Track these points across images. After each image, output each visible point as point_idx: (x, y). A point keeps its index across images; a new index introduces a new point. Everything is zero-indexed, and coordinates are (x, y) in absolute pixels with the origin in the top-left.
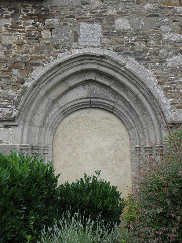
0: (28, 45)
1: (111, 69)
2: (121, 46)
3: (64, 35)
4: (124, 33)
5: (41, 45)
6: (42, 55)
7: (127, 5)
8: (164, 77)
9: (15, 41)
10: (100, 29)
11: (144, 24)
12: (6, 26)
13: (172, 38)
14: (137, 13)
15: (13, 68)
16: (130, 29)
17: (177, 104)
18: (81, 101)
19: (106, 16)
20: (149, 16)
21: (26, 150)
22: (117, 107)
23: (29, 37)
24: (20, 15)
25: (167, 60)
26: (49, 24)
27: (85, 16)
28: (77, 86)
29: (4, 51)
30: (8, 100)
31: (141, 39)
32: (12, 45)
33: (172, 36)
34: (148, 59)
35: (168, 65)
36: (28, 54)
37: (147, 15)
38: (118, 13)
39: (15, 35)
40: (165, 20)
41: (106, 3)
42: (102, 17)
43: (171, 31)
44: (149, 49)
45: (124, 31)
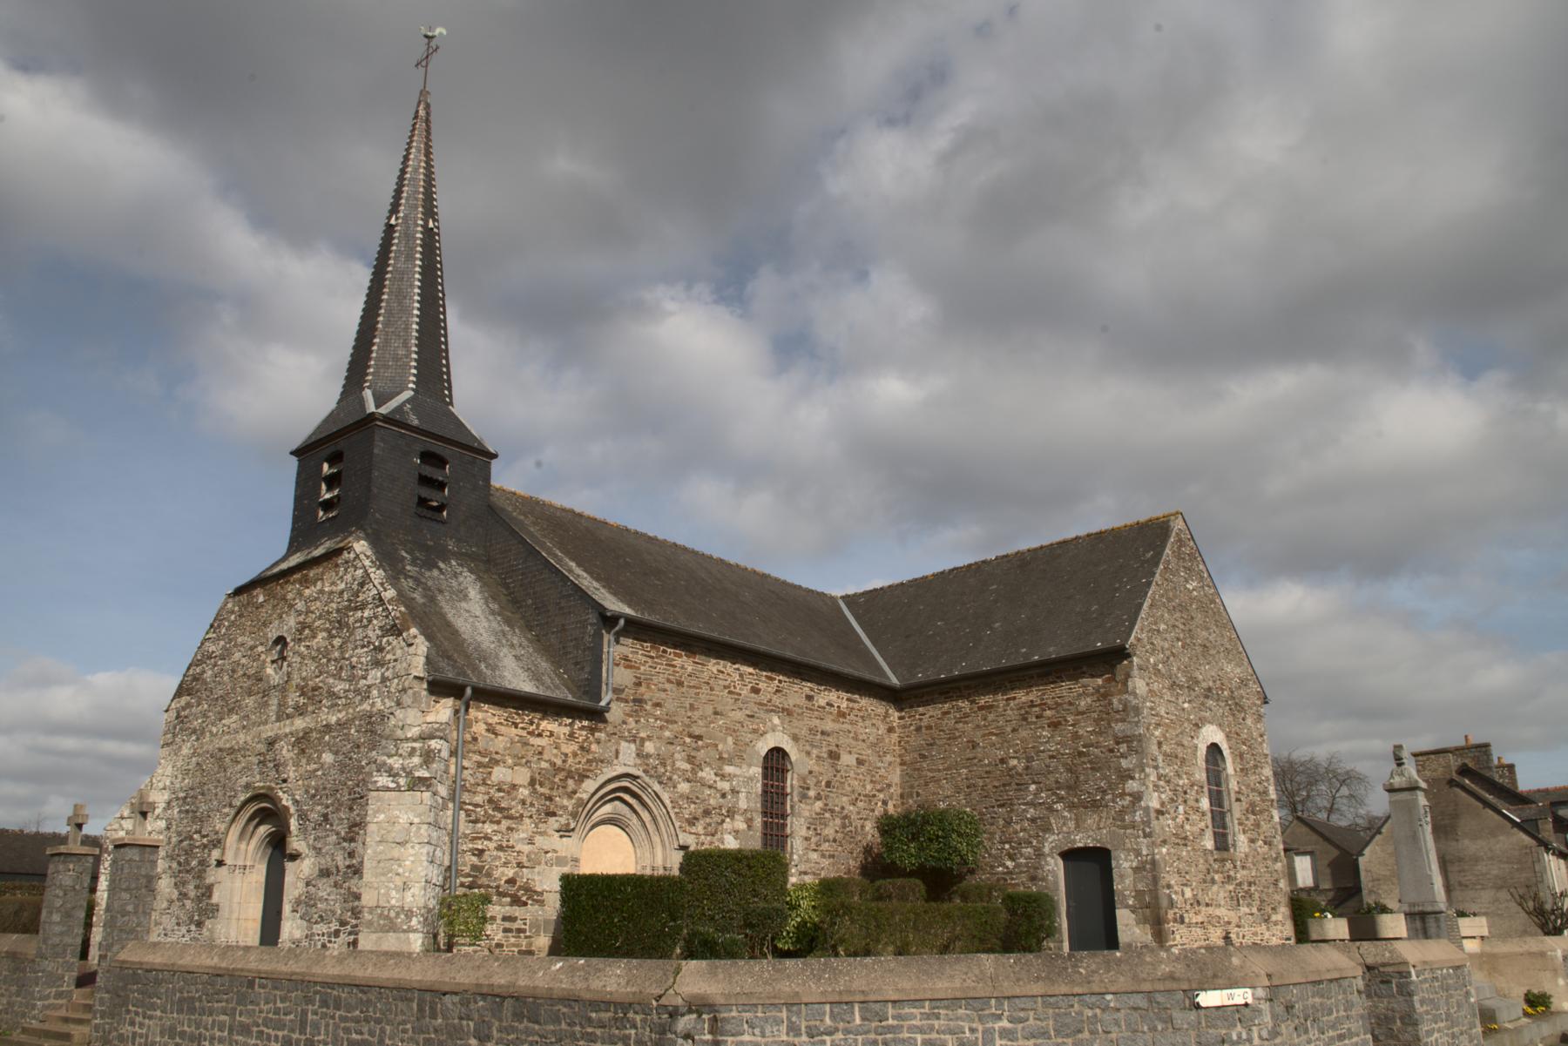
21: (1453, 868)
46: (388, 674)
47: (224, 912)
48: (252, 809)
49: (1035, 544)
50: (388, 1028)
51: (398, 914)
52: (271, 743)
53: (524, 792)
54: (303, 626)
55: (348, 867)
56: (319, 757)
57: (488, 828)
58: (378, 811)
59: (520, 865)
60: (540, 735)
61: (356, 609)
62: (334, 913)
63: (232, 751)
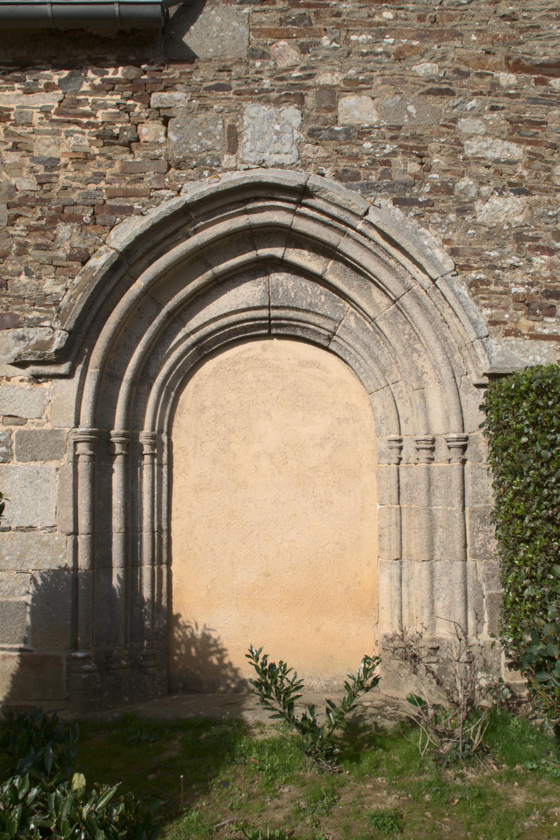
0: (103, 159)
1: (325, 224)
2: (354, 167)
3: (200, 134)
4: (363, 133)
5: (139, 160)
6: (140, 186)
7: (370, 62)
8: (471, 251)
9: (67, 150)
10: (297, 121)
11: (414, 112)
12: (45, 111)
13: (490, 150)
14: (398, 83)
15: (58, 220)
16: (378, 123)
17: (505, 323)
18: (244, 315)
19: (315, 87)
20: (429, 92)
22: (341, 335)
23: (108, 139)
24: (84, 82)
25: (477, 208)
26: (160, 106)
27: (260, 87)
28: (234, 276)
29: (36, 176)
30: (44, 306)
31: (407, 151)
32: (59, 160)
33: (489, 146)
34: (428, 203)
35: (479, 220)
36: (102, 184)
37: (422, 90)
38: (345, 80)
39: (69, 134)
40: (469, 104)
41: (315, 56)
42: (305, 90)
43: (486, 134)
44: (430, 176)
45: (363, 128)
47: (182, 613)
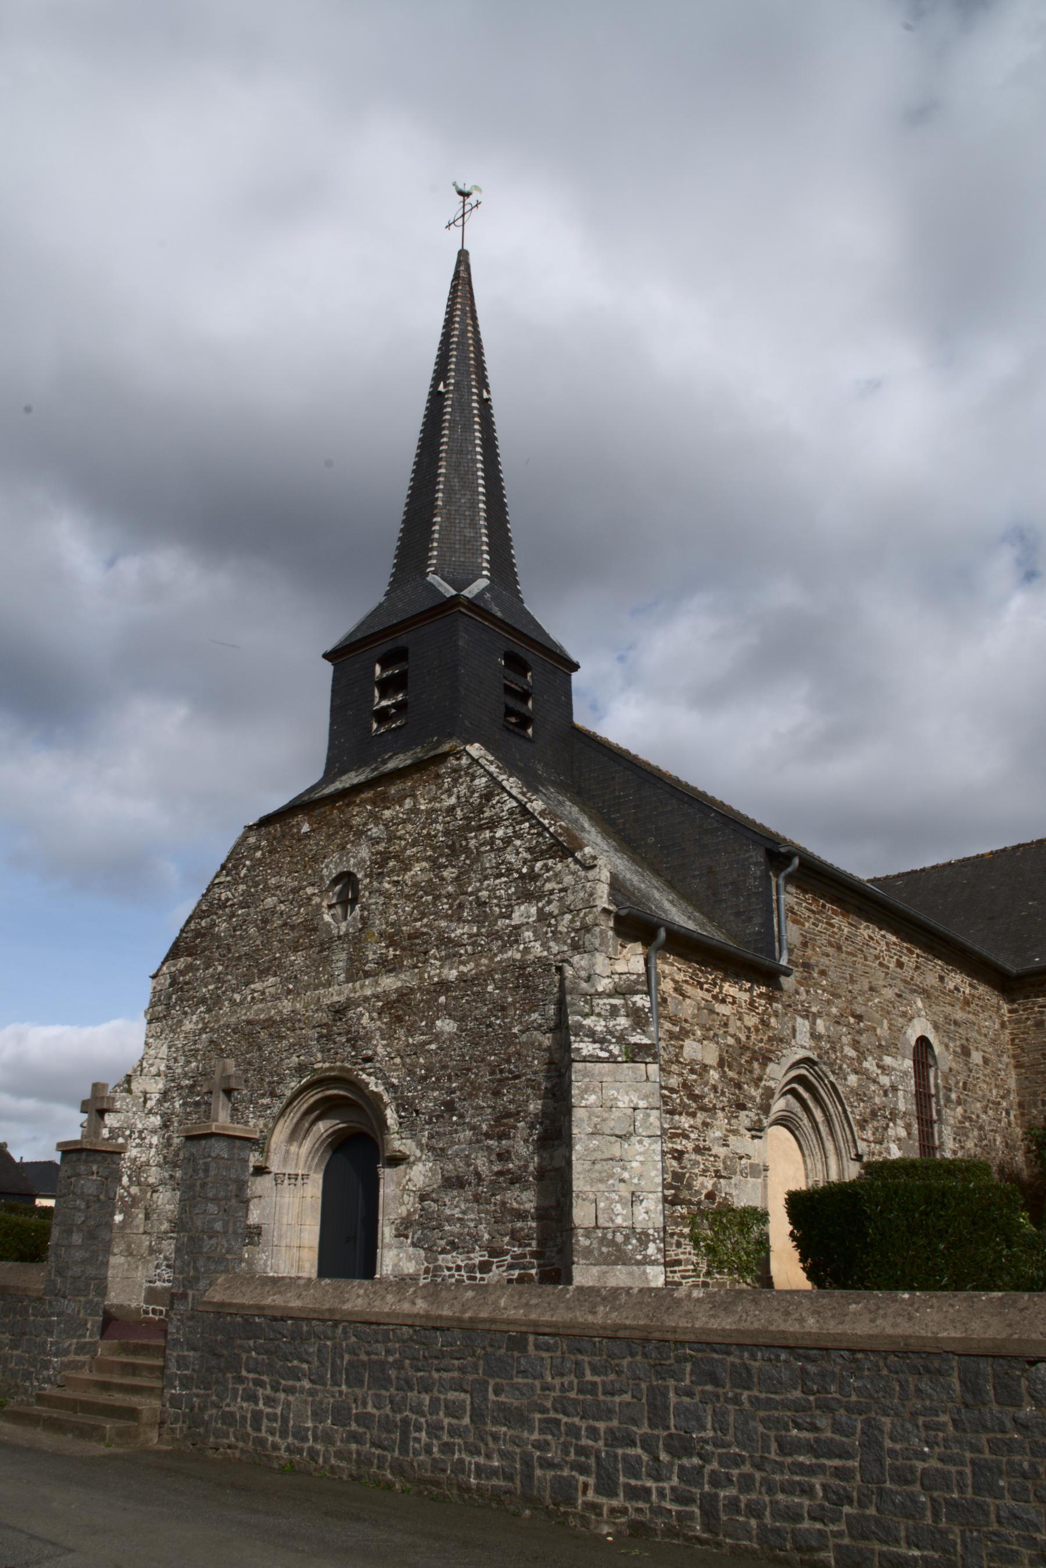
46: (553, 908)
48: (313, 1097)
49: (941, 860)
50: (887, 1422)
51: (627, 1238)
52: (339, 1011)
53: (714, 1075)
54: (384, 858)
55: (499, 1173)
56: (431, 1025)
57: (685, 1122)
58: (586, 1090)
59: (718, 1175)
60: (723, 1001)
61: (480, 828)
62: (476, 1238)
63: (269, 1023)
